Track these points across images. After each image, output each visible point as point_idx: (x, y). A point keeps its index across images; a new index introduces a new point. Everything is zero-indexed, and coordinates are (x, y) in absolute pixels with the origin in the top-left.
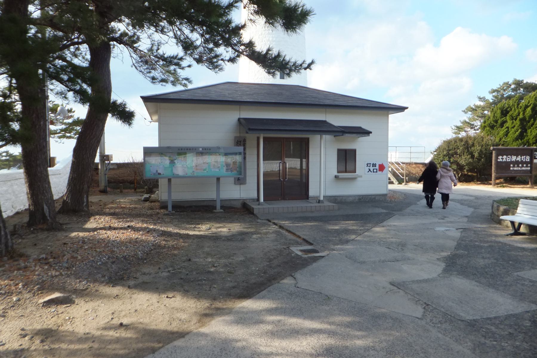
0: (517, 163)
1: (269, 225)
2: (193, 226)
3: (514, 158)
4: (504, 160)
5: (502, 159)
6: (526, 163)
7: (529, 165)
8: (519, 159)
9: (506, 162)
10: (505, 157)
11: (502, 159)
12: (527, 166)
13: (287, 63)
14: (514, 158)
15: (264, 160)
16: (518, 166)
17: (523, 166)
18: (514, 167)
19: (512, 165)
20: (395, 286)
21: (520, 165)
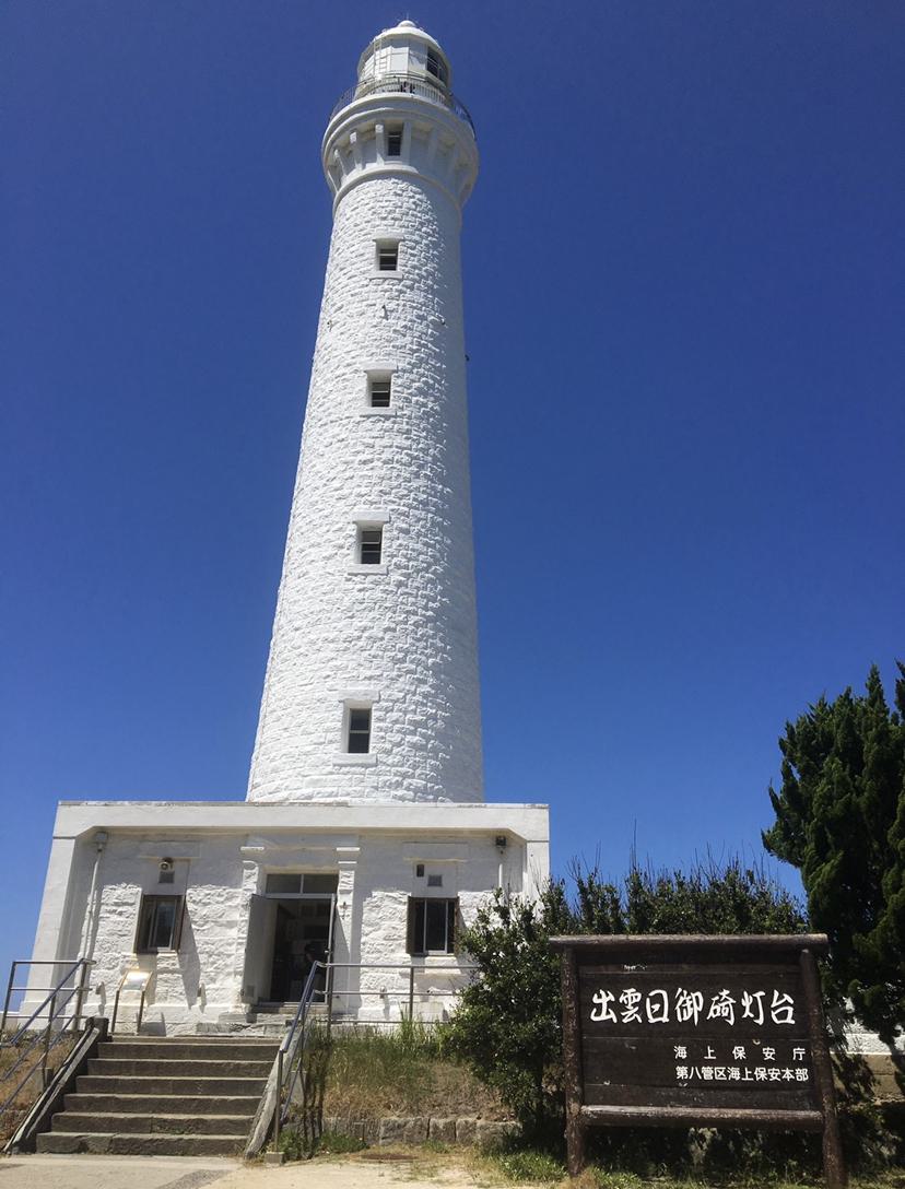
0: (709, 1037)
1: (326, 1125)
2: (483, 804)
3: (691, 1006)
4: (630, 1015)
5: (618, 1007)
6: (771, 1033)
7: (799, 1052)
8: (722, 1008)
9: (641, 1028)
10: (631, 996)
11: (618, 1007)
12: (783, 1060)
13: (460, 1058)
14: (691, 1006)
15: (75, 1092)
16: (726, 1060)
17: (754, 1059)
18: (695, 1060)
19: (681, 1052)
20: (264, 804)
21: (769, 1053)
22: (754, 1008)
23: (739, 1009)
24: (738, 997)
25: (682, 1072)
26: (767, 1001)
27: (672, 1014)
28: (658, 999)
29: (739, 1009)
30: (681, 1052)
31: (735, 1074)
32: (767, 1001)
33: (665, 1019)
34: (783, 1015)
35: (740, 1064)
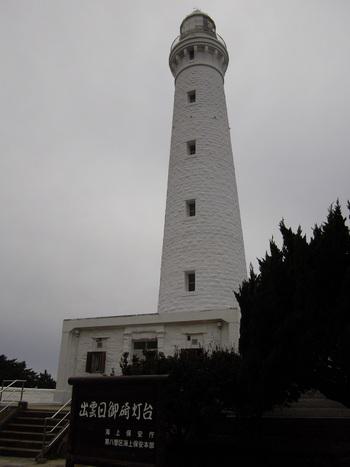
0: (119, 424)
5: (89, 410)
7: (152, 434)
14: (114, 409)
17: (134, 437)
19: (108, 432)
22: (137, 412)
23: (131, 411)
24: (131, 406)
25: (107, 441)
26: (142, 407)
27: (107, 414)
28: (102, 407)
29: (131, 411)
30: (108, 432)
31: (126, 444)
32: (142, 407)
33: (104, 416)
34: (147, 415)
35: (128, 439)
